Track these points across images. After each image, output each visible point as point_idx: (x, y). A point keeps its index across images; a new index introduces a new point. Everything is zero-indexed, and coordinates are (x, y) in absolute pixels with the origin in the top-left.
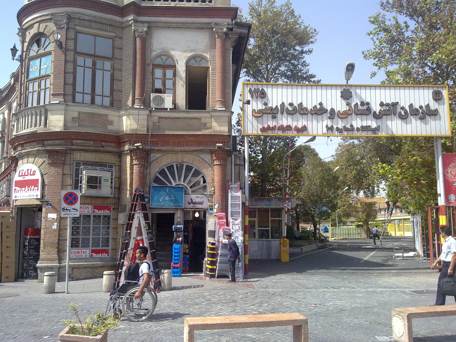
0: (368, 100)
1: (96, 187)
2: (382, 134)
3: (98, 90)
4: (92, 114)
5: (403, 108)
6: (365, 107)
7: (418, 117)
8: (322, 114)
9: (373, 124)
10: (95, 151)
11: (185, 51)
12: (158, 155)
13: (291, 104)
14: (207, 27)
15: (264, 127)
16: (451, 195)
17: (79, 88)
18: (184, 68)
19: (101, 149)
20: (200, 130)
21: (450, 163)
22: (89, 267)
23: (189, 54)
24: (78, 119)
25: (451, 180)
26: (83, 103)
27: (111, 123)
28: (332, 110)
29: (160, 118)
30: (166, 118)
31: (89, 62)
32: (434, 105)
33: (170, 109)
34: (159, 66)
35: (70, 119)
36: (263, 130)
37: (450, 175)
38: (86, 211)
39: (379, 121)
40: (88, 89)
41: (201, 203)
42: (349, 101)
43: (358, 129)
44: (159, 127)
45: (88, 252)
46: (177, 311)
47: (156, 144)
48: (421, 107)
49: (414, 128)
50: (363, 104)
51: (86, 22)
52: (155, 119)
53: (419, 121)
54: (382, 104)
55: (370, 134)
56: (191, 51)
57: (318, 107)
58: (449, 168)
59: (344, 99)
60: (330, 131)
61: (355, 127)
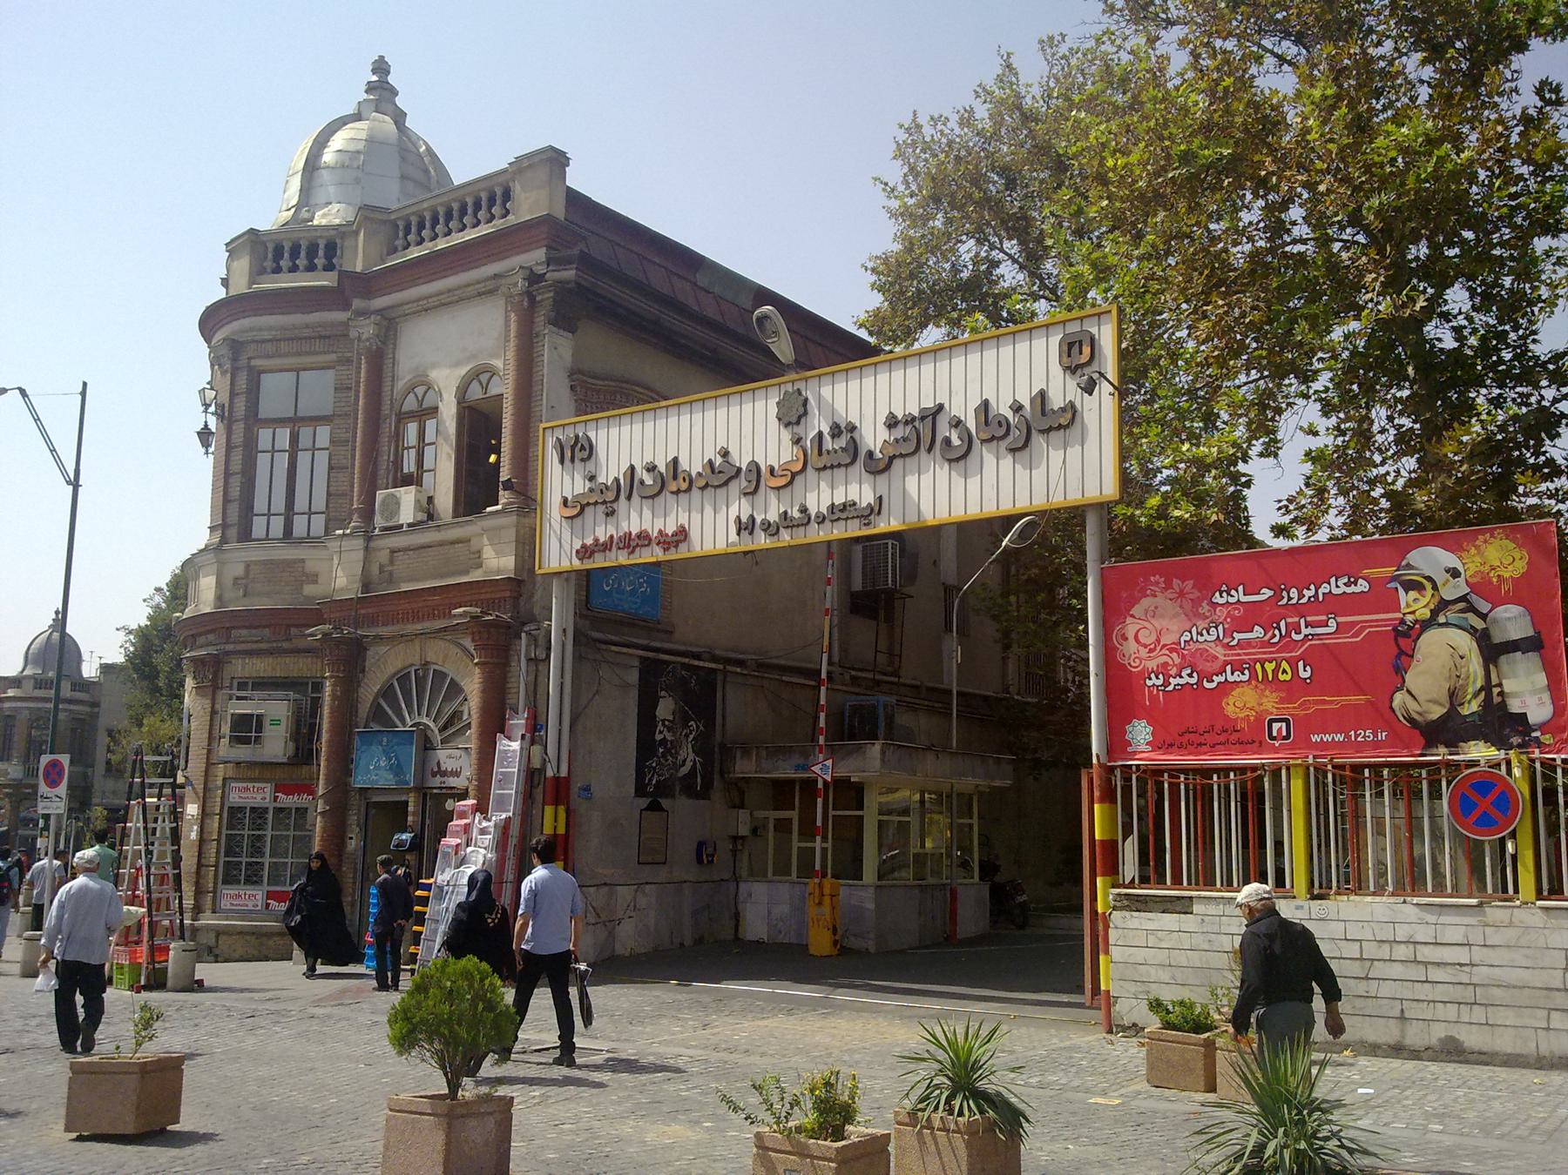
0: (854, 418)
1: (246, 741)
2: (888, 523)
3: (301, 503)
4: (271, 562)
5: (957, 423)
6: (842, 442)
7: (1003, 444)
8: (726, 483)
9: (861, 491)
10: (270, 652)
11: (457, 364)
12: (383, 649)
13: (651, 468)
14: (486, 292)
15: (584, 546)
16: (1135, 722)
17: (260, 505)
18: (454, 410)
19: (285, 645)
20: (466, 572)
21: (1133, 602)
22: (247, 933)
23: (463, 371)
24: (244, 583)
25: (1135, 666)
26: (267, 538)
27: (313, 578)
28: (755, 467)
29: (393, 552)
30: (406, 549)
31: (284, 435)
32: (1062, 390)
33: (410, 525)
34: (412, 415)
35: (228, 582)
36: (585, 552)
37: (1131, 646)
38: (259, 797)
39: (882, 480)
40: (279, 504)
41: (457, 774)
42: (799, 430)
43: (821, 520)
44: (391, 574)
45: (259, 897)
46: (1309, 925)
47: (373, 621)
48: (1017, 408)
49: (996, 488)
50: (836, 431)
51: (269, 345)
52: (383, 557)
53: (1007, 461)
54: (892, 423)
55: (854, 530)
56: (468, 360)
57: (718, 461)
58: (1129, 620)
59: (787, 425)
60: (745, 534)
61: (813, 512)
